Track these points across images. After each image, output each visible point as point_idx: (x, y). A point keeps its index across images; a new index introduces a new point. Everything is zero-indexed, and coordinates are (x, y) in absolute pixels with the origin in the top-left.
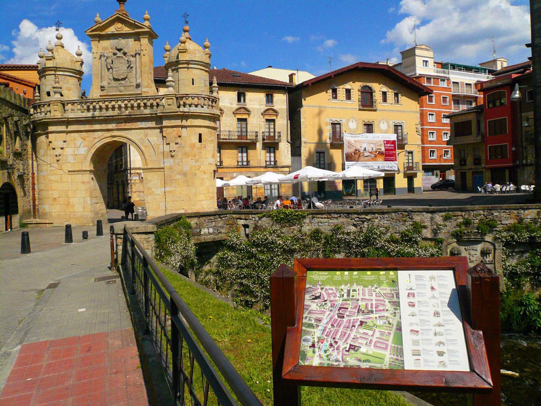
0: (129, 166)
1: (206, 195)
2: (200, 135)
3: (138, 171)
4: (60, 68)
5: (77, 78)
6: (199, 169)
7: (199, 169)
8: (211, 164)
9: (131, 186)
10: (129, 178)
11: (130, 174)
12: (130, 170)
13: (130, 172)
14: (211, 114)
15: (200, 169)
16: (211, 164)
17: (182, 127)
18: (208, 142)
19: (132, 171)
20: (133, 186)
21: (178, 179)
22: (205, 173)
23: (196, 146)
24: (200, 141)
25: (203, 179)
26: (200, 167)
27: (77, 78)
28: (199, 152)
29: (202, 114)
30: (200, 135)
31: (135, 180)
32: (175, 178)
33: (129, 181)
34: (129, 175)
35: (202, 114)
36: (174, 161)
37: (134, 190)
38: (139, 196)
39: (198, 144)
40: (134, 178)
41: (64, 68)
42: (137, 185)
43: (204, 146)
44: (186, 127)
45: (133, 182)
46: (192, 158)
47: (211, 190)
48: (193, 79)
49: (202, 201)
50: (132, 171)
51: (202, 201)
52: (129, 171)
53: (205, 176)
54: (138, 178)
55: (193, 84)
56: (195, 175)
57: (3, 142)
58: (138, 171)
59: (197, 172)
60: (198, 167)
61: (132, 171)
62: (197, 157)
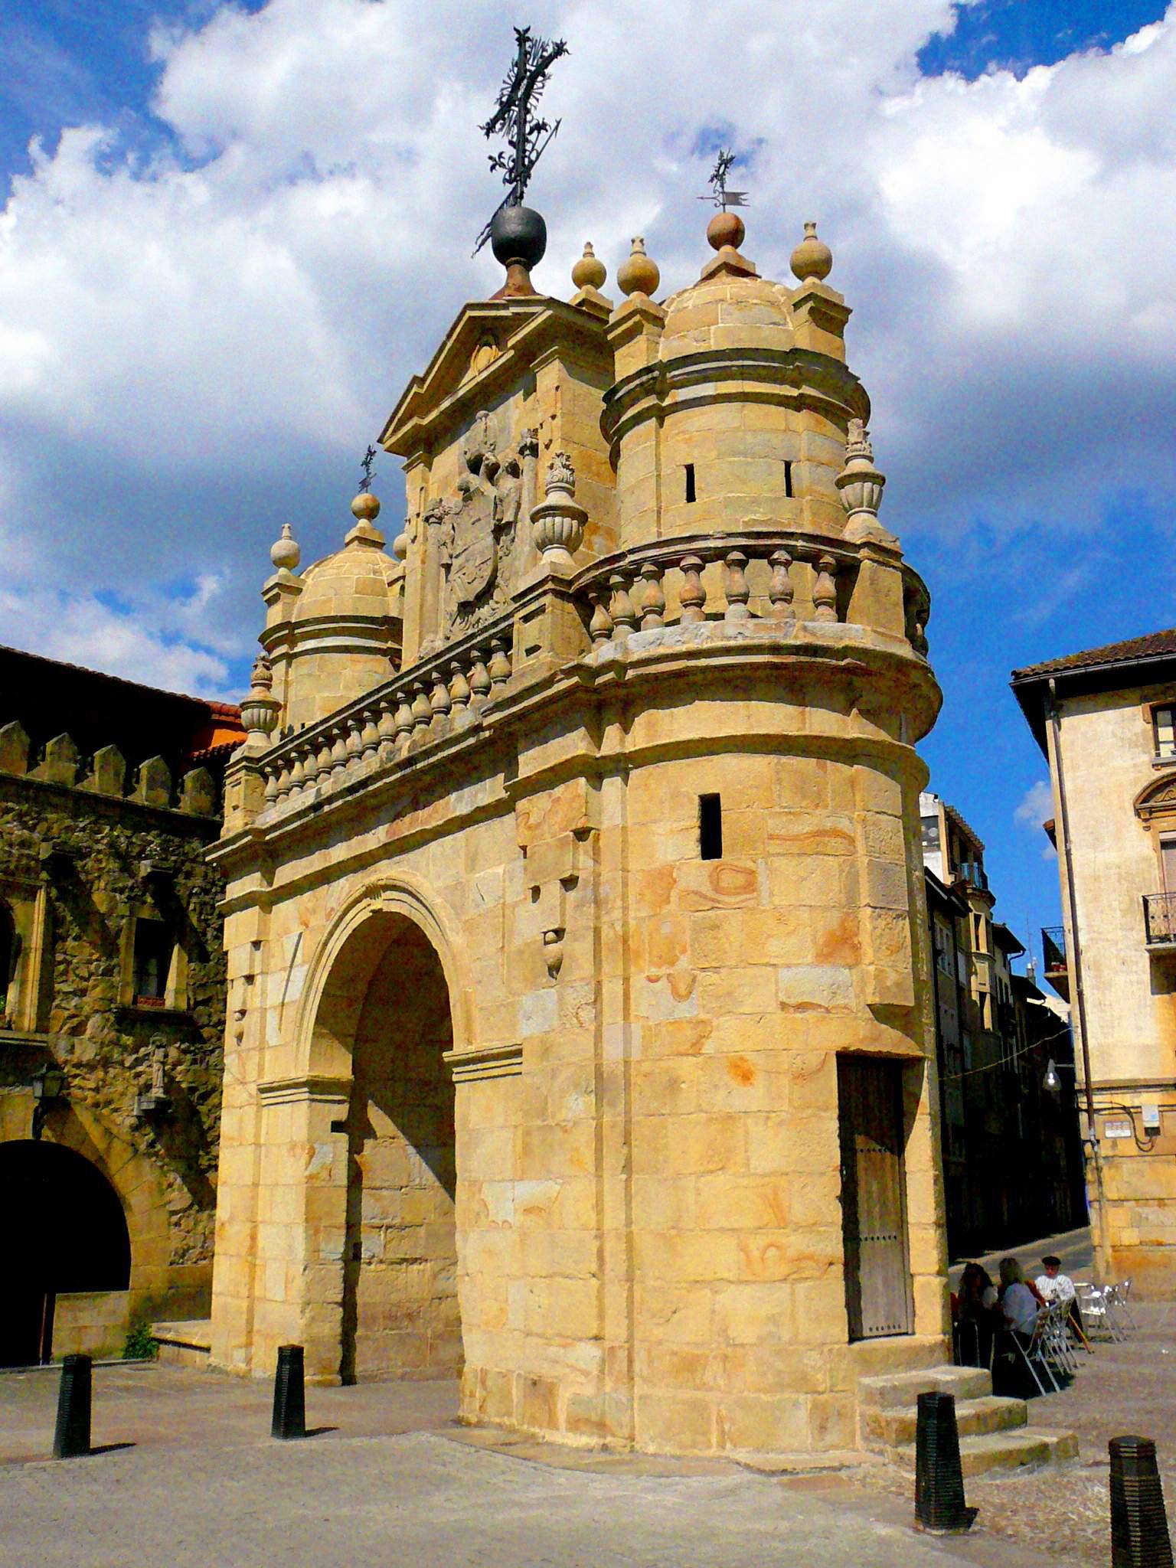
0: (1080, 1075)
1: (755, 1244)
2: (710, 807)
3: (1126, 1099)
4: (307, 622)
5: (383, 652)
6: (695, 1048)
7: (695, 1048)
8: (801, 1007)
9: (1098, 1169)
10: (1085, 1134)
11: (1091, 1111)
12: (1088, 1091)
13: (1090, 1103)
14: (775, 649)
15: (708, 1048)
16: (801, 1007)
17: (597, 771)
18: (774, 847)
19: (1096, 1098)
20: (1106, 1174)
21: (575, 1123)
22: (746, 1077)
23: (682, 885)
24: (711, 845)
25: (729, 1117)
26: (702, 1030)
27: (383, 652)
28: (698, 930)
29: (703, 662)
30: (710, 807)
31: (1114, 1142)
32: (563, 1115)
33: (1088, 1148)
34: (1083, 1118)
35: (703, 662)
36: (561, 1000)
37: (1111, 1191)
38: (1137, 1222)
39: (696, 870)
40: (1109, 1133)
41: (344, 619)
42: (1127, 1166)
43: (741, 880)
44: (622, 765)
45: (1104, 1150)
46: (654, 971)
47: (798, 1211)
48: (690, 469)
49: (715, 1285)
50: (1100, 1100)
51: (715, 1285)
52: (1083, 1100)
53: (754, 1097)
54: (1128, 1133)
55: (691, 497)
56: (673, 1085)
57: (25, 966)
58: (1126, 1099)
59: (686, 1067)
60: (689, 1033)
61: (1100, 1100)
62: (684, 963)
